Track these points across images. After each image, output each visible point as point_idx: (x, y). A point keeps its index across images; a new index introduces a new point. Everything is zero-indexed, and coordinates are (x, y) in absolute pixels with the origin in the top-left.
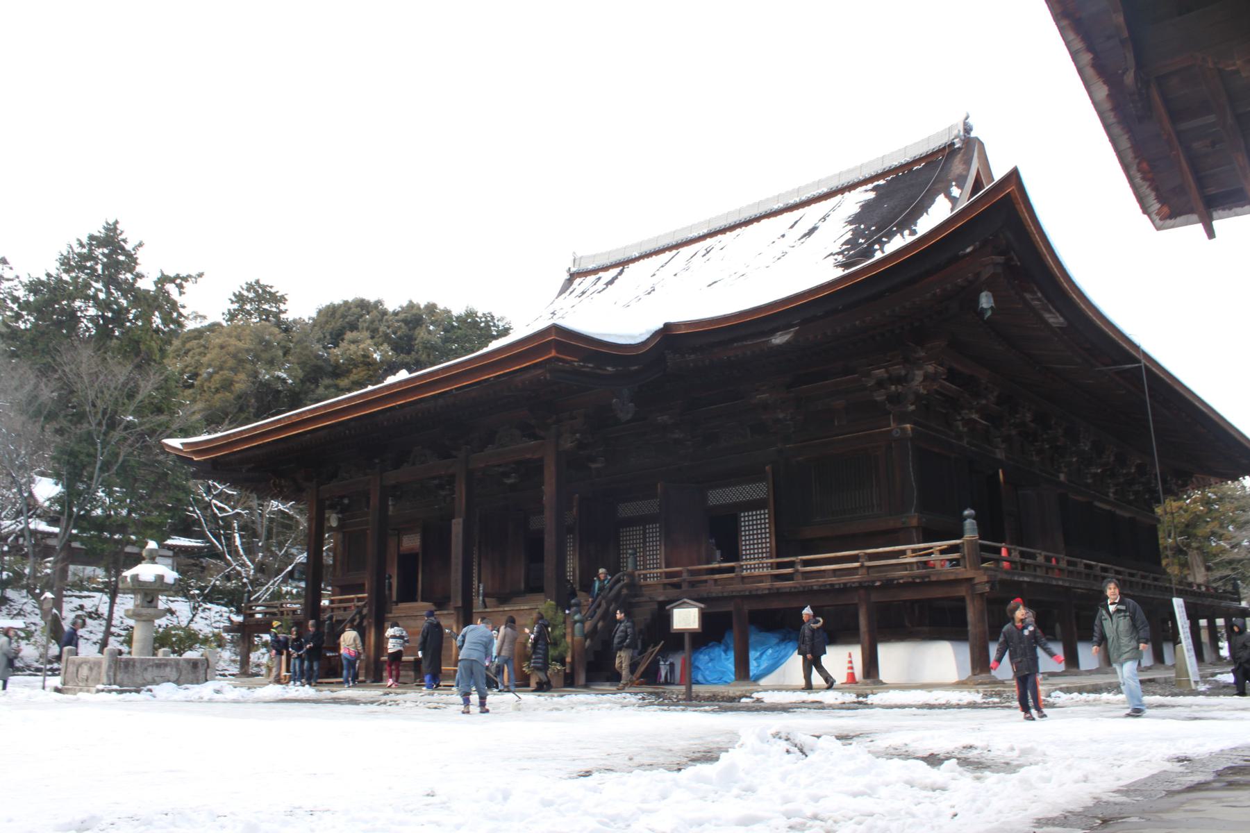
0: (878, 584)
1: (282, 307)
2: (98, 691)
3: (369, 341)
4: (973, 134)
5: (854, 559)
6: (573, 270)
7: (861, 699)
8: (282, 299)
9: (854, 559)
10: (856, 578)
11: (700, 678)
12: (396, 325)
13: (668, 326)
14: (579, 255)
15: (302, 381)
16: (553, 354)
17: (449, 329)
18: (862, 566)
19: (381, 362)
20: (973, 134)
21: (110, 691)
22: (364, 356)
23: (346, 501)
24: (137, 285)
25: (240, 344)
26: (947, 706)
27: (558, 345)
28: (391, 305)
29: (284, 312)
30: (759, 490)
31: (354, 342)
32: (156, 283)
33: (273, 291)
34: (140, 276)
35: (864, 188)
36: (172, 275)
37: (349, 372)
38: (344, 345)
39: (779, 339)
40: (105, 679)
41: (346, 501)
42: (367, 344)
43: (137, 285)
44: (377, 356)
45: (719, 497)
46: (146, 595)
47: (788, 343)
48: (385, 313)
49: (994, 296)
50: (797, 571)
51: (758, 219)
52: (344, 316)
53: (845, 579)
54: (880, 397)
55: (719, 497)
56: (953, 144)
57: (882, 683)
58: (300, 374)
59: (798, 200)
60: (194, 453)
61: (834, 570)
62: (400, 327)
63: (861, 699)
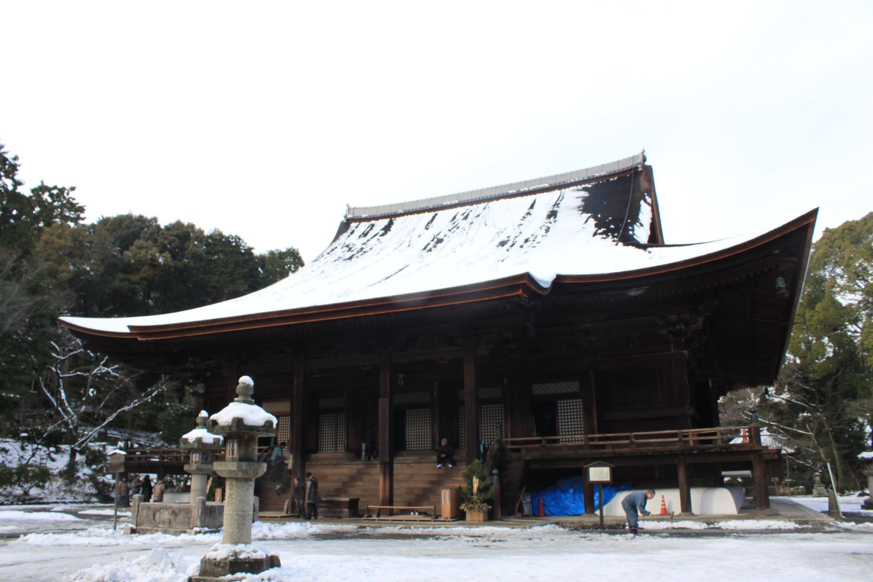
0: (695, 452)
1: (82, 215)
2: (197, 533)
3: (155, 249)
4: (647, 163)
5: (675, 435)
6: (350, 216)
7: (712, 526)
8: (81, 209)
9: (675, 435)
10: (676, 447)
11: (547, 511)
12: (171, 238)
13: (559, 277)
14: (352, 206)
15: (102, 275)
16: (520, 292)
17: (208, 245)
18: (680, 440)
19: (164, 265)
20: (647, 163)
21: (205, 533)
22: (152, 259)
23: (208, 374)
24: (18, 191)
25: (62, 242)
26: (779, 531)
27: (524, 287)
28: (163, 223)
29: (83, 219)
30: (573, 386)
31: (141, 248)
32: (33, 191)
33: (74, 202)
34: (20, 184)
35: (575, 188)
36: (51, 185)
37: (139, 270)
38: (133, 248)
39: (633, 293)
40: (199, 523)
41: (208, 374)
42: (155, 251)
43: (18, 191)
44: (161, 260)
45: (540, 389)
46: (203, 454)
47: (641, 295)
48: (158, 227)
49: (785, 281)
50: (632, 442)
51: (498, 198)
52: (128, 227)
53: (668, 448)
54: (663, 332)
55: (540, 389)
56: (637, 168)
57: (693, 514)
58: (102, 268)
59: (527, 189)
60: (140, 334)
61: (659, 443)
62: (174, 241)
63: (712, 526)
